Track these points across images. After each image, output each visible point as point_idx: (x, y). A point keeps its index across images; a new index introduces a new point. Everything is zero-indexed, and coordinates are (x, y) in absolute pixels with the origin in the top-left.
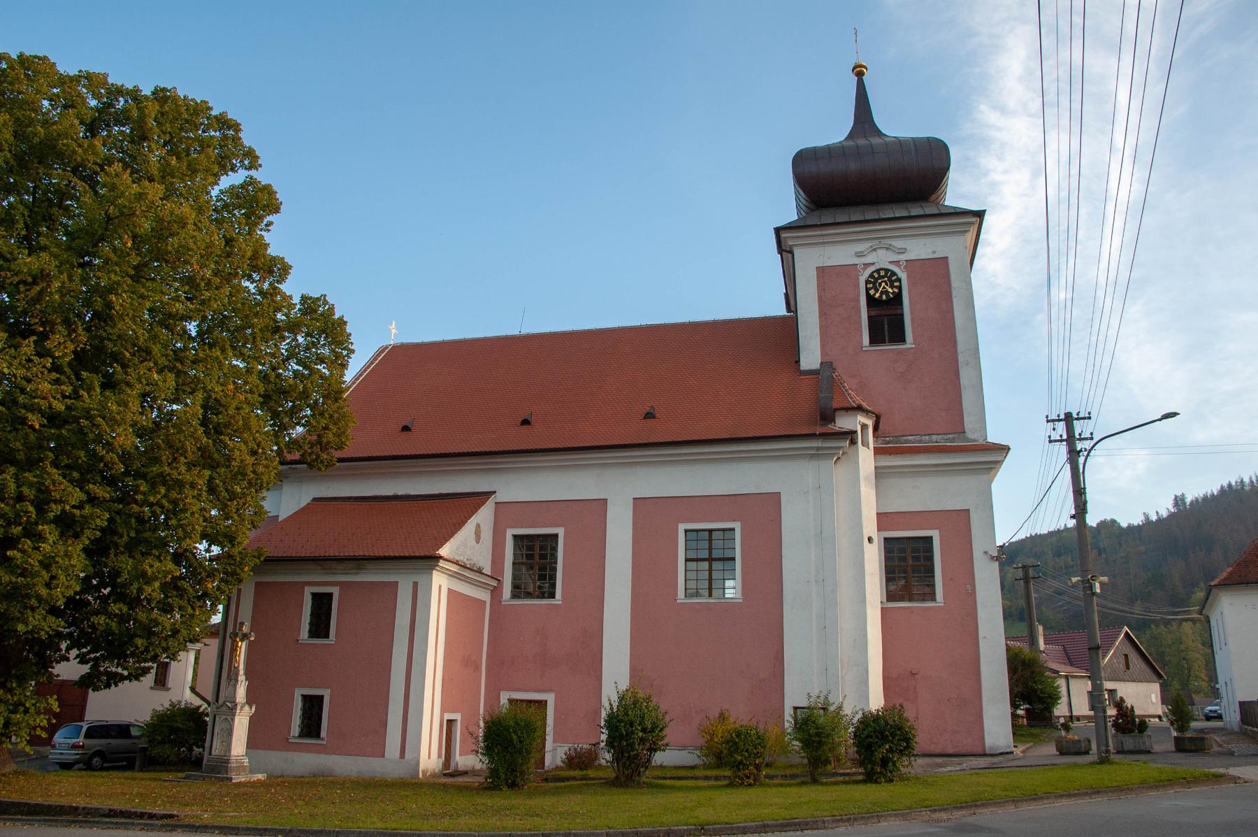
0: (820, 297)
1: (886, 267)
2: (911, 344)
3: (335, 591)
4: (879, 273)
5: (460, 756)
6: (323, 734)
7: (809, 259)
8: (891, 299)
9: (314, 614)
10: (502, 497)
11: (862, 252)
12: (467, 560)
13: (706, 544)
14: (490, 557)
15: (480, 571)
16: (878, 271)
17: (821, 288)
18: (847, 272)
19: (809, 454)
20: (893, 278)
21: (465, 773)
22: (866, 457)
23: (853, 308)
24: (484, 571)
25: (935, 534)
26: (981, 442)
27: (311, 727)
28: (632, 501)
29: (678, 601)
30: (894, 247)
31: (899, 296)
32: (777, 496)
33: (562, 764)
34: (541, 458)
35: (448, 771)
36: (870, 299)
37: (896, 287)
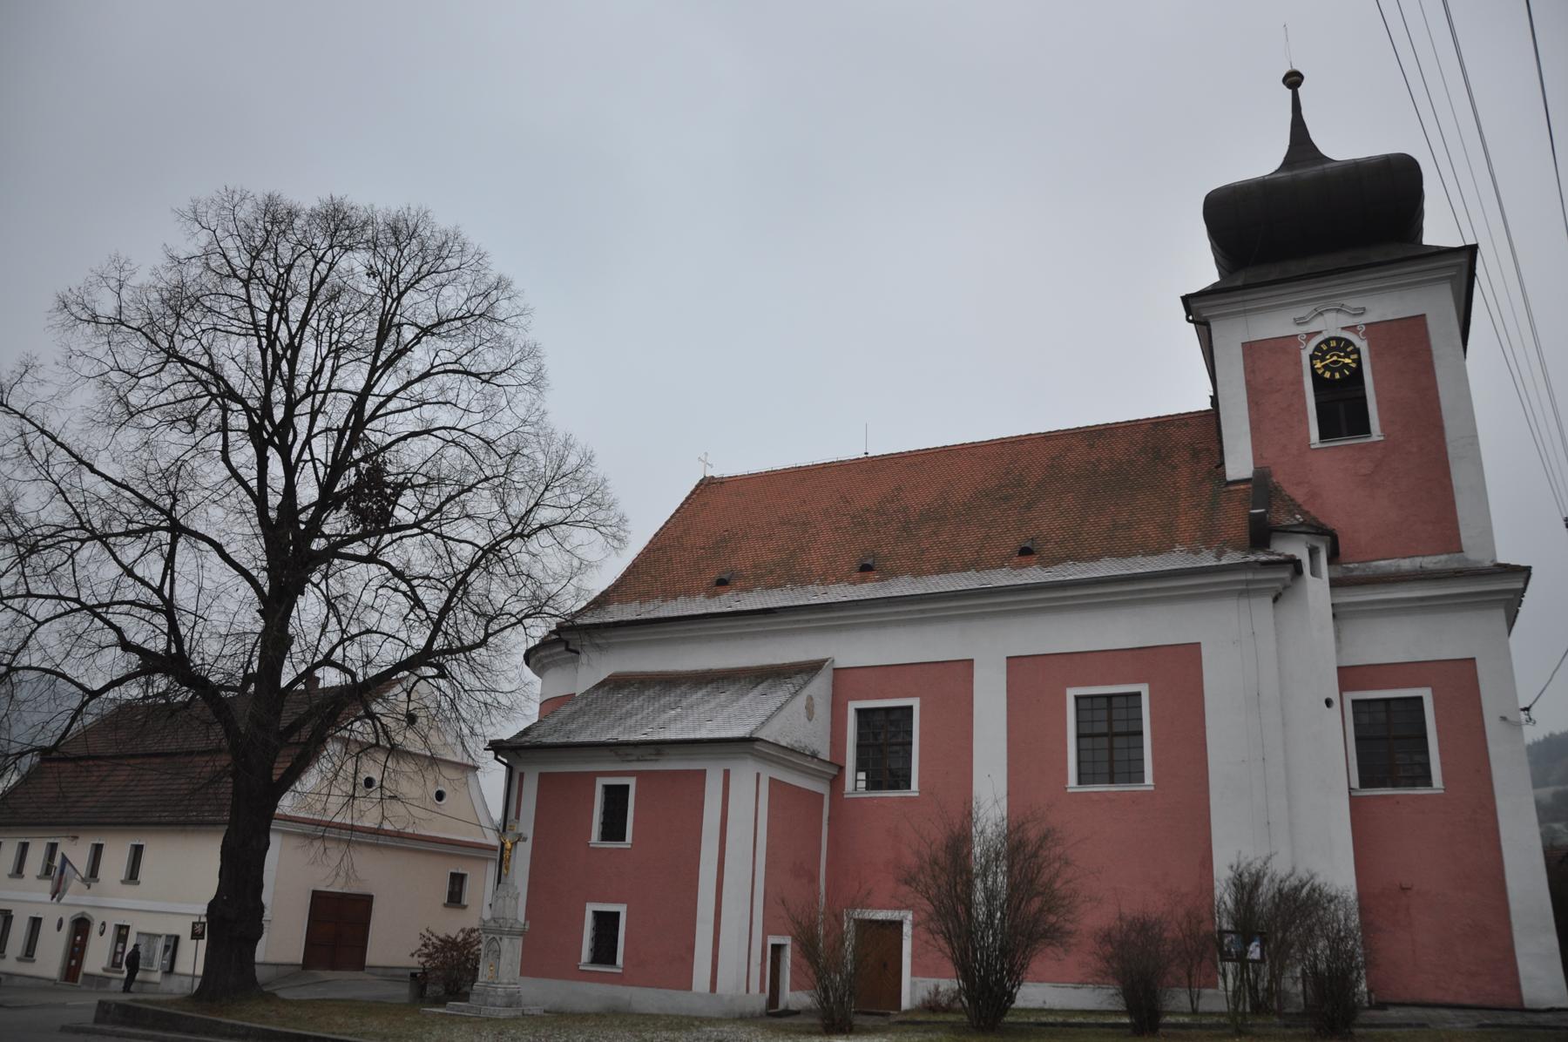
0: (1248, 383)
1: (1338, 335)
3: (631, 782)
5: (791, 990)
6: (620, 960)
7: (1232, 336)
9: (607, 813)
10: (842, 662)
11: (1304, 318)
12: (796, 741)
14: (828, 739)
15: (814, 756)
16: (1327, 341)
17: (1250, 371)
18: (1287, 346)
21: (797, 1013)
22: (1317, 589)
25: (1426, 694)
26: (1488, 564)
27: (604, 950)
28: (1005, 659)
29: (1069, 790)
30: (1349, 308)
31: (1358, 373)
32: (1195, 647)
34: (701, 626)
35: (776, 1010)
36: (1316, 377)
37: (1352, 352)
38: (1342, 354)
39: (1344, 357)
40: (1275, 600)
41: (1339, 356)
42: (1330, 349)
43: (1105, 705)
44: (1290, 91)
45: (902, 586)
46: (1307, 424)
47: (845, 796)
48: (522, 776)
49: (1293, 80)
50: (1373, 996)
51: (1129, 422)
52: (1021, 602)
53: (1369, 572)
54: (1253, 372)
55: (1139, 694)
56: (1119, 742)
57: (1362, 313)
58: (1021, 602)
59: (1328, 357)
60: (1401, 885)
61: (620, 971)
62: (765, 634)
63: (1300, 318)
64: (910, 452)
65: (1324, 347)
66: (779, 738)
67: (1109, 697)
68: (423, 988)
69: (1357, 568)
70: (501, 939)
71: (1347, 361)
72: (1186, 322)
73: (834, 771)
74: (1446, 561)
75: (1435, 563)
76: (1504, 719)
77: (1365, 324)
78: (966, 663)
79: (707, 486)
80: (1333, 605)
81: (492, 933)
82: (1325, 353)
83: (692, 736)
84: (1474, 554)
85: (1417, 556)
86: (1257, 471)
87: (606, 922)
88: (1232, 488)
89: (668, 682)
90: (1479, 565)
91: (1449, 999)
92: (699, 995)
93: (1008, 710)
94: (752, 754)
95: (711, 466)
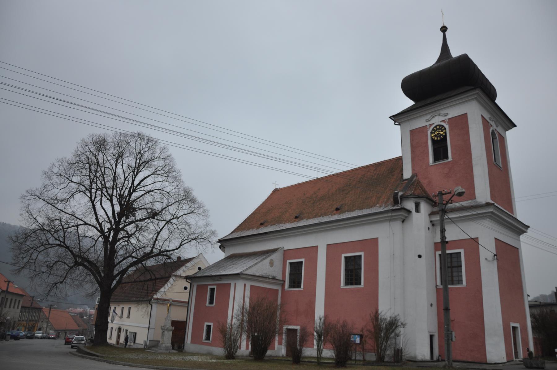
2: (451, 159)
8: (442, 138)
11: (428, 119)
16: (436, 127)
18: (423, 129)
20: (441, 127)
23: (425, 146)
24: (277, 278)
28: (326, 246)
29: (341, 288)
31: (445, 137)
33: (88, 313)
36: (433, 140)
37: (444, 130)
40: (403, 221)
42: (437, 129)
44: (443, 33)
47: (285, 290)
49: (444, 29)
50: (440, 357)
51: (390, 159)
54: (413, 140)
56: (454, 269)
57: (447, 115)
63: (427, 120)
66: (256, 273)
71: (442, 133)
72: (394, 125)
73: (282, 282)
75: (467, 204)
76: (486, 259)
77: (448, 119)
79: (276, 191)
80: (431, 221)
82: (435, 131)
85: (461, 202)
87: (209, 327)
90: (481, 203)
91: (464, 359)
95: (278, 185)
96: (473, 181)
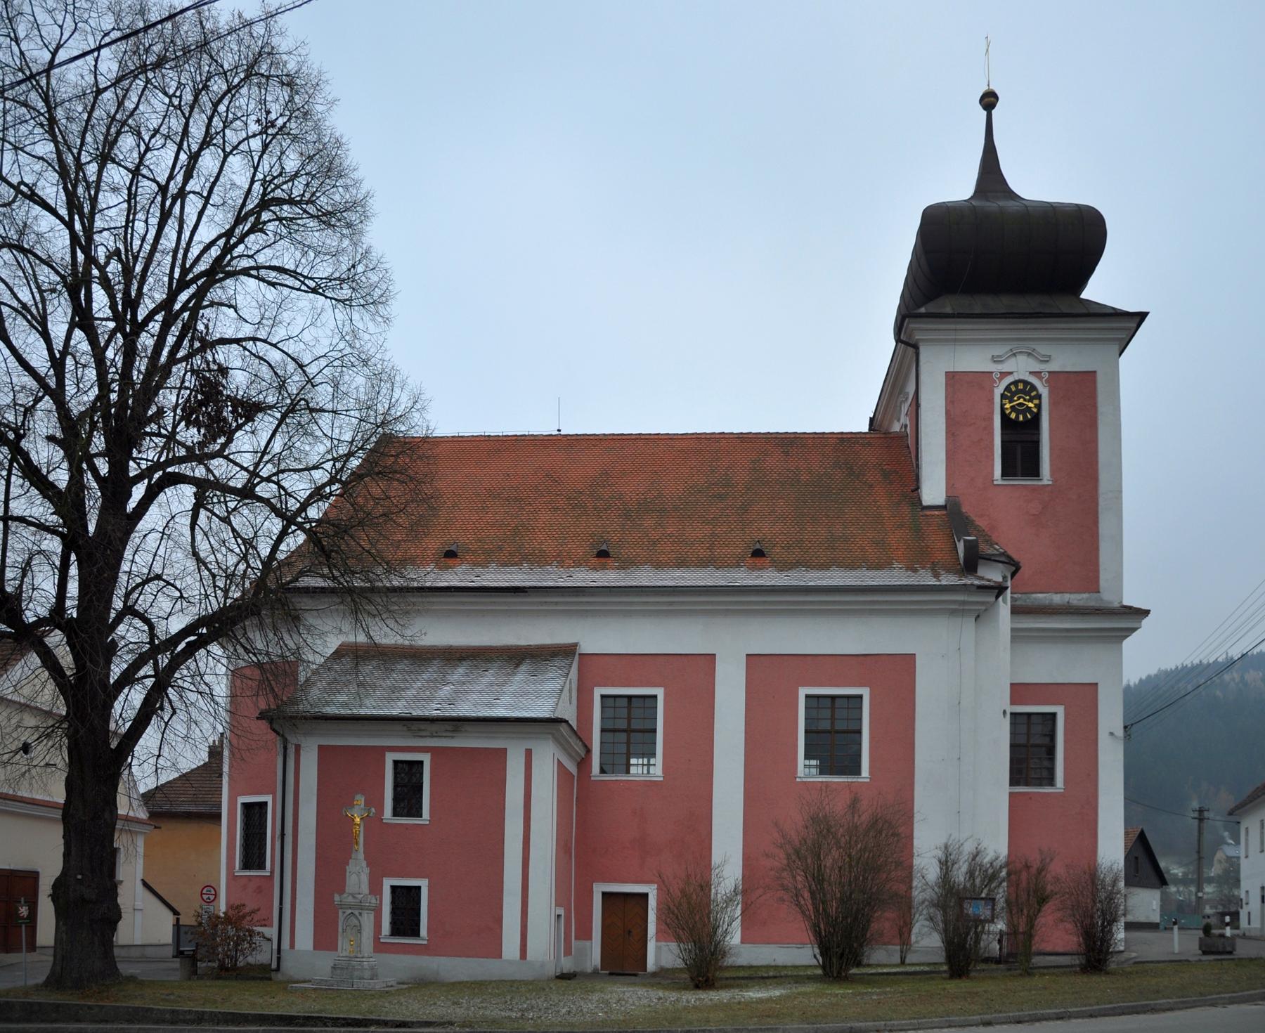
0: (948, 413)
3: (426, 758)
4: (1016, 387)
13: (624, 713)
16: (1015, 383)
17: (951, 401)
18: (982, 380)
19: (949, 609)
25: (1060, 710)
26: (1116, 605)
30: (1039, 353)
31: (1037, 418)
32: (912, 657)
34: (442, 599)
36: (1004, 417)
38: (1028, 397)
39: (1029, 401)
41: (1025, 400)
42: (1018, 391)
43: (829, 705)
45: (645, 577)
46: (993, 460)
47: (592, 779)
48: (298, 748)
49: (989, 101)
52: (765, 603)
53: (1029, 603)
55: (860, 697)
57: (1048, 361)
58: (765, 603)
59: (1015, 398)
60: (1026, 864)
61: (425, 942)
62: (508, 613)
64: (604, 435)
65: (1013, 389)
67: (833, 698)
68: (194, 965)
69: (1020, 598)
70: (360, 914)
71: (1031, 405)
74: (1087, 599)
75: (1080, 600)
76: (1112, 734)
77: (1049, 372)
78: (708, 657)
81: (350, 908)
82: (1014, 394)
83: (487, 714)
84: (1107, 596)
86: (949, 498)
88: (928, 513)
89: (419, 656)
90: (1111, 605)
92: (510, 962)
93: (747, 704)
94: (553, 734)
96: (1097, 549)
